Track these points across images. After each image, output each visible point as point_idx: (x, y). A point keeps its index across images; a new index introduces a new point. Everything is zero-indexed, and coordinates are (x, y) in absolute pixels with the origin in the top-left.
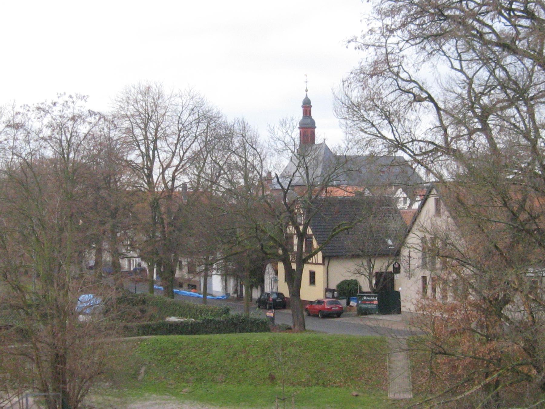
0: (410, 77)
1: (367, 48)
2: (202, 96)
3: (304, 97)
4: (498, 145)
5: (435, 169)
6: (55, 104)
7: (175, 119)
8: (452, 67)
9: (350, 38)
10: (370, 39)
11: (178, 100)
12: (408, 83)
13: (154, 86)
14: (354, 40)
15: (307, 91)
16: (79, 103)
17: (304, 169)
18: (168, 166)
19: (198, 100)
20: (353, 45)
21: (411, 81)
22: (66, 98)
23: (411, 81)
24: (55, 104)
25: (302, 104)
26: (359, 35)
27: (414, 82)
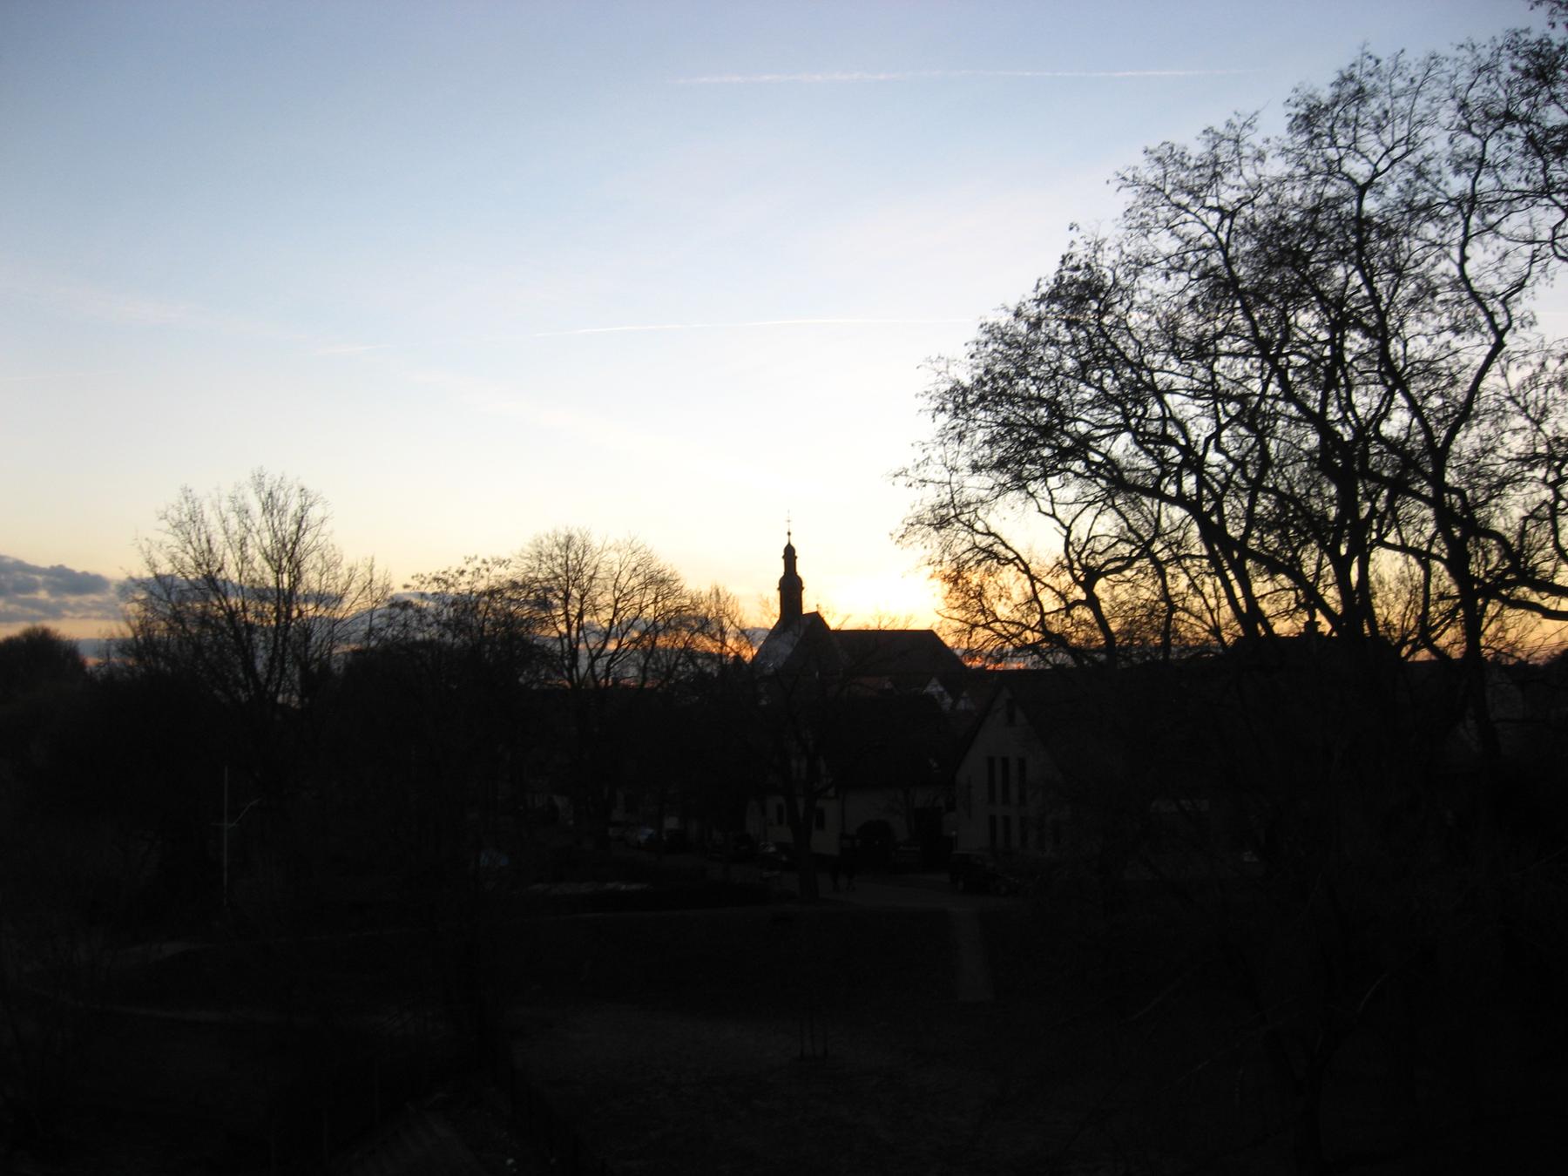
6: (462, 573)
7: (611, 583)
11: (613, 556)
13: (577, 536)
16: (498, 571)
17: (593, 600)
18: (598, 656)
20: (902, 480)
21: (989, 534)
22: (478, 564)
23: (989, 534)
24: (462, 573)
26: (910, 465)
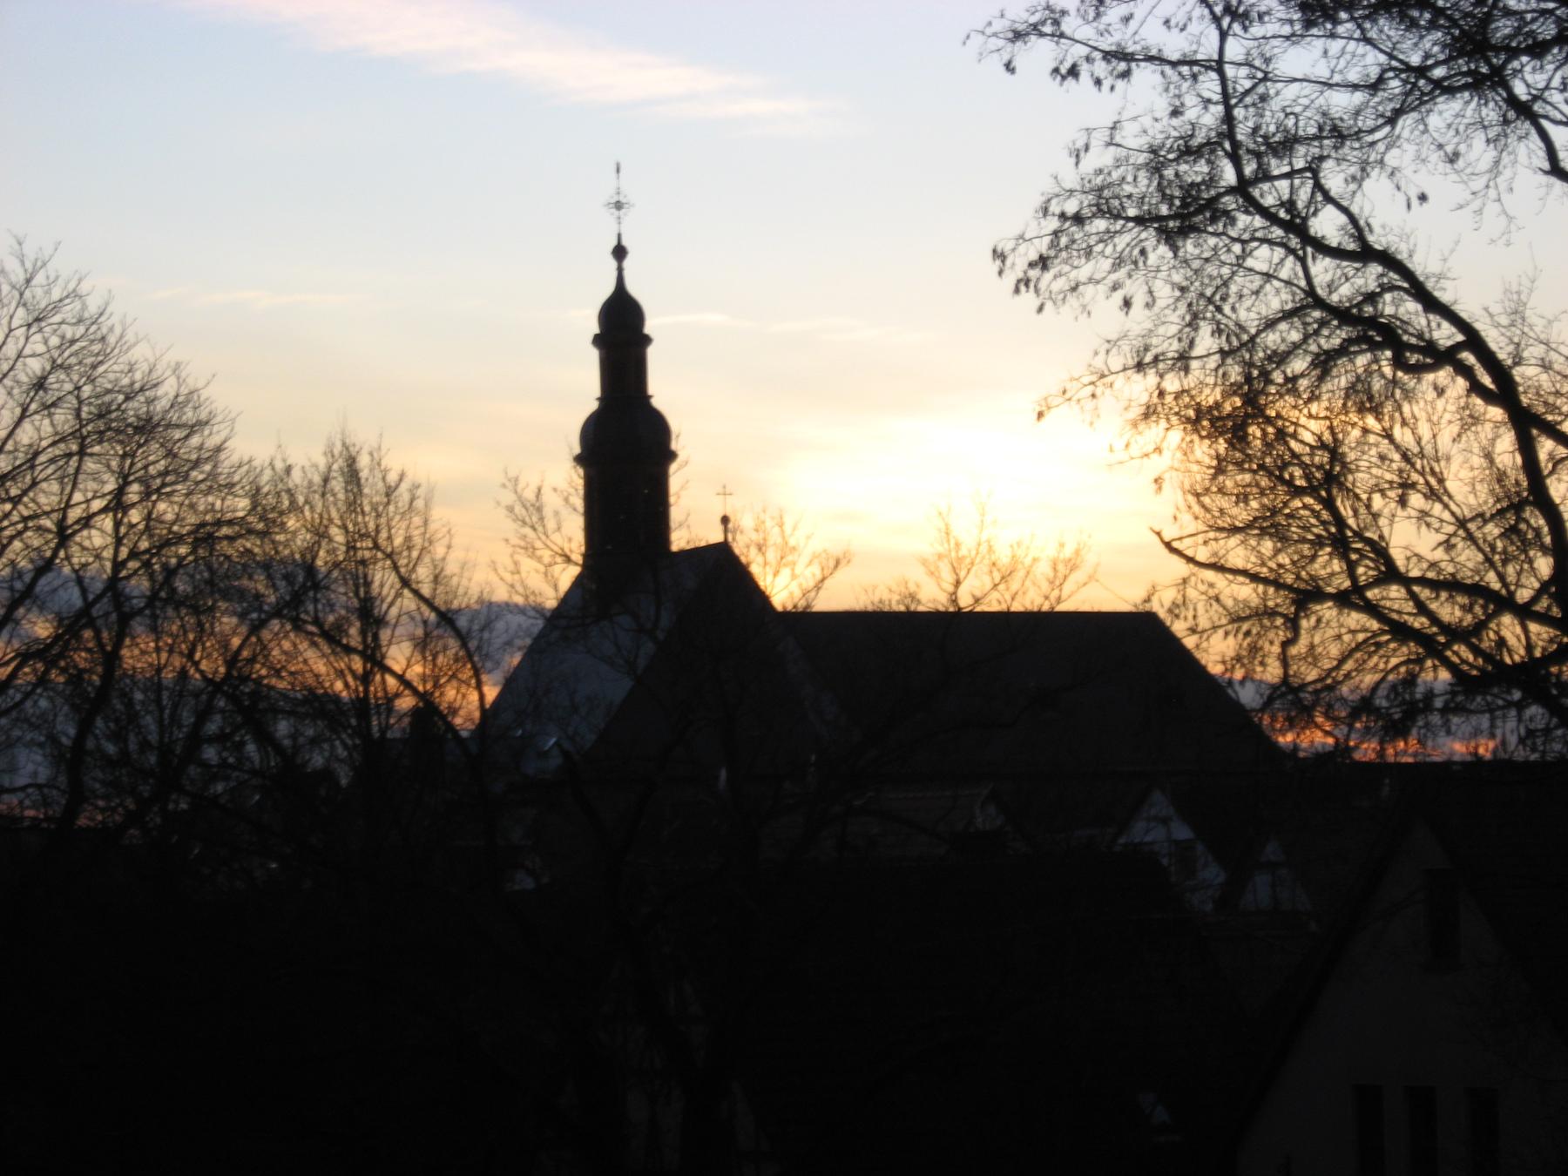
0: (1360, 237)
1: (1126, 75)
2: (93, 309)
3: (608, 289)
5: (1351, 631)
12: (1349, 267)
15: (620, 252)
19: (69, 332)
21: (1366, 253)
23: (1366, 253)
25: (594, 328)
27: (1387, 259)
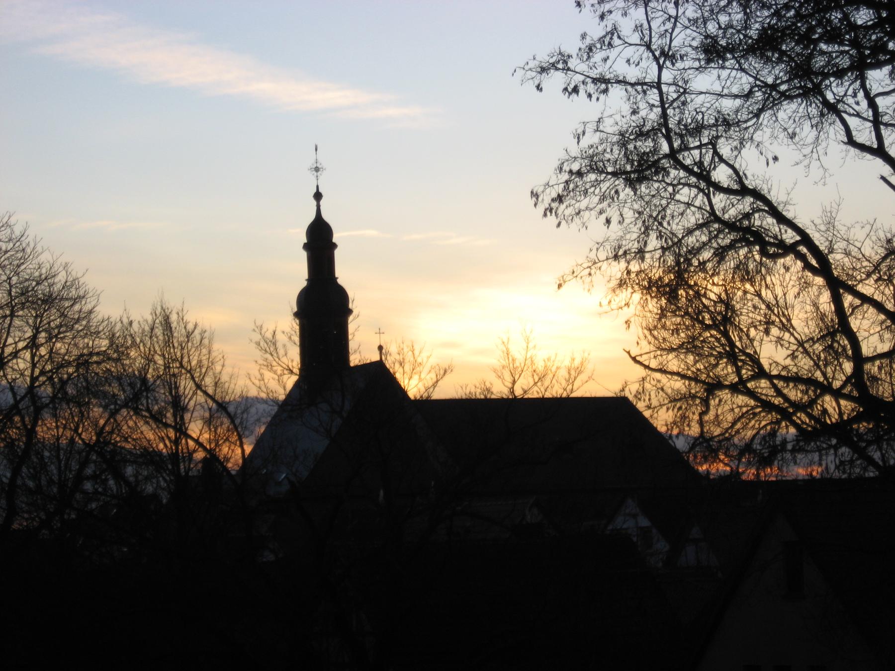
4: (752, 200)
8: (851, 141)
9: (544, 57)
10: (605, 60)
12: (734, 199)
14: (561, 63)
15: (318, 196)
21: (743, 191)
26: (572, 46)
27: (756, 194)
